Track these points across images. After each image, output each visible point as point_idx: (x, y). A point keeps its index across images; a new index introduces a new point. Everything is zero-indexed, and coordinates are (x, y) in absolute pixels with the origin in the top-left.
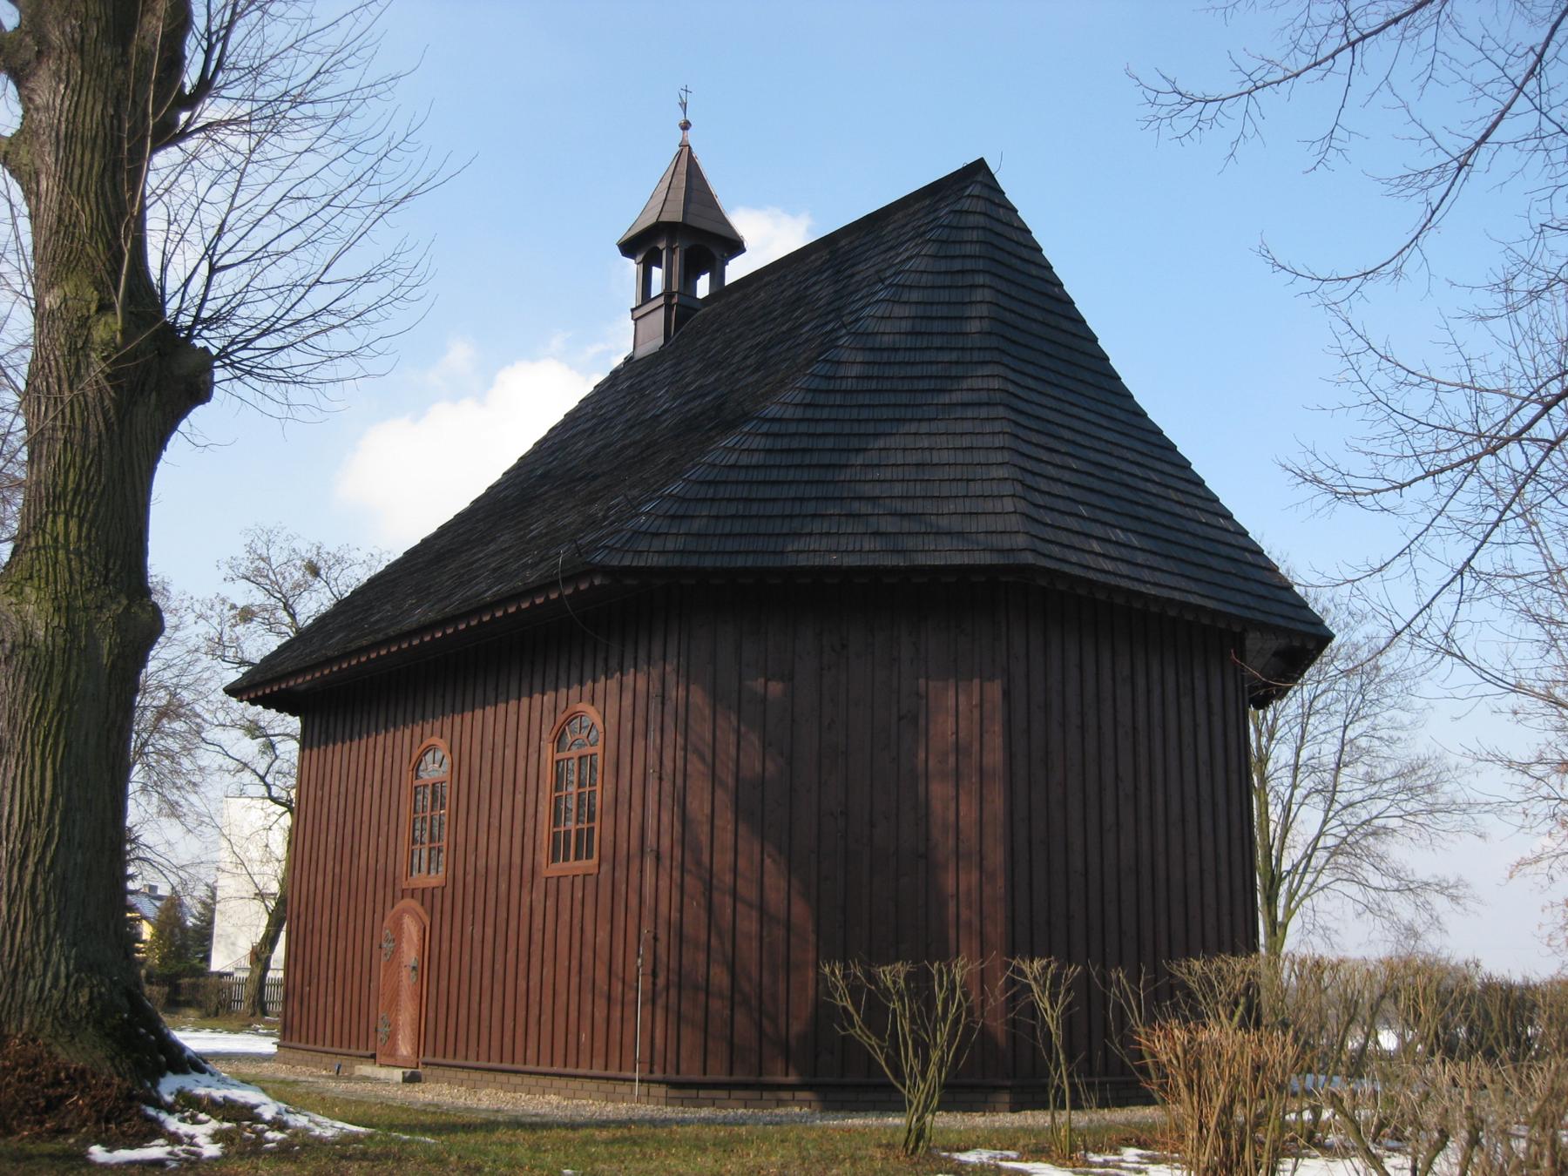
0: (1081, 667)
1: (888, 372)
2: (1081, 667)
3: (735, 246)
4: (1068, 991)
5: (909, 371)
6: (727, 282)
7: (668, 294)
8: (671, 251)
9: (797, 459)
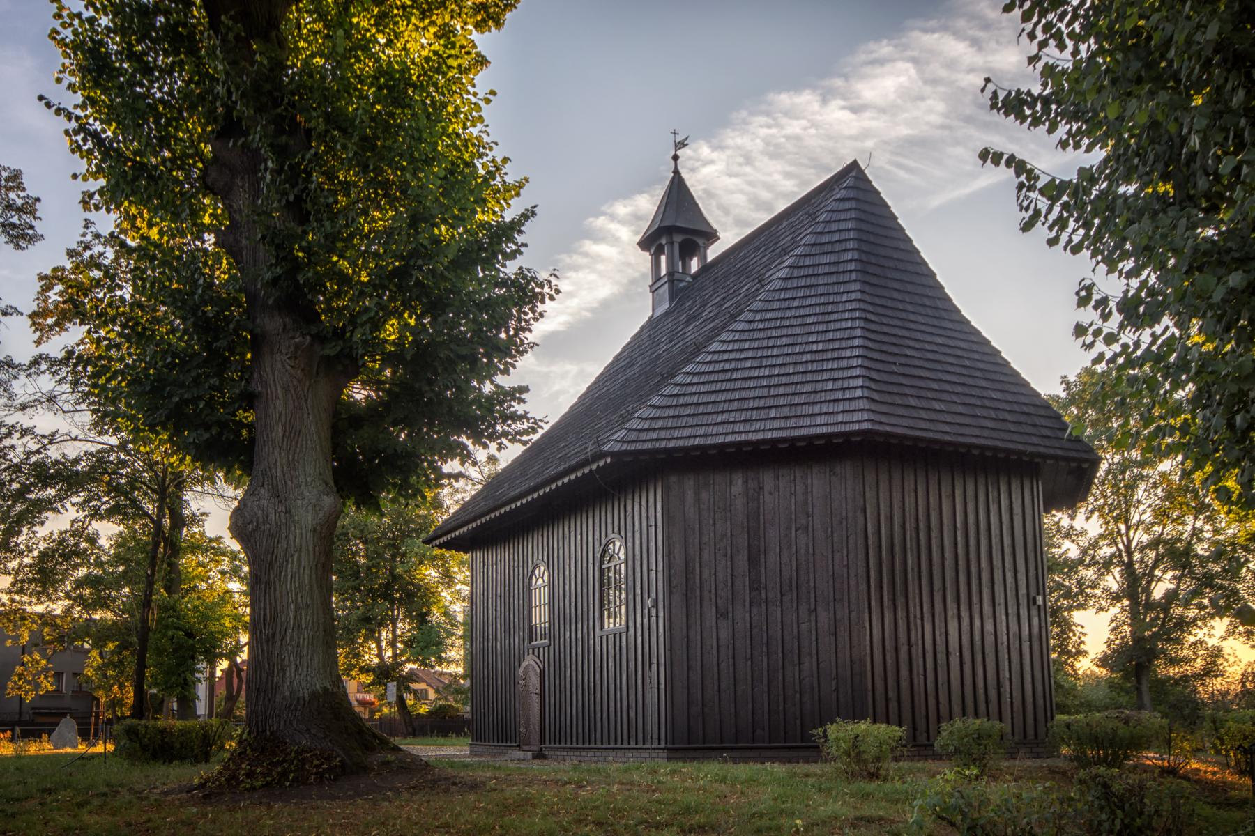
0: (887, 700)
1: (788, 314)
2: (887, 700)
3: (711, 236)
4: (871, 52)
5: (801, 312)
6: (709, 260)
7: (670, 273)
8: (671, 243)
9: (728, 376)
